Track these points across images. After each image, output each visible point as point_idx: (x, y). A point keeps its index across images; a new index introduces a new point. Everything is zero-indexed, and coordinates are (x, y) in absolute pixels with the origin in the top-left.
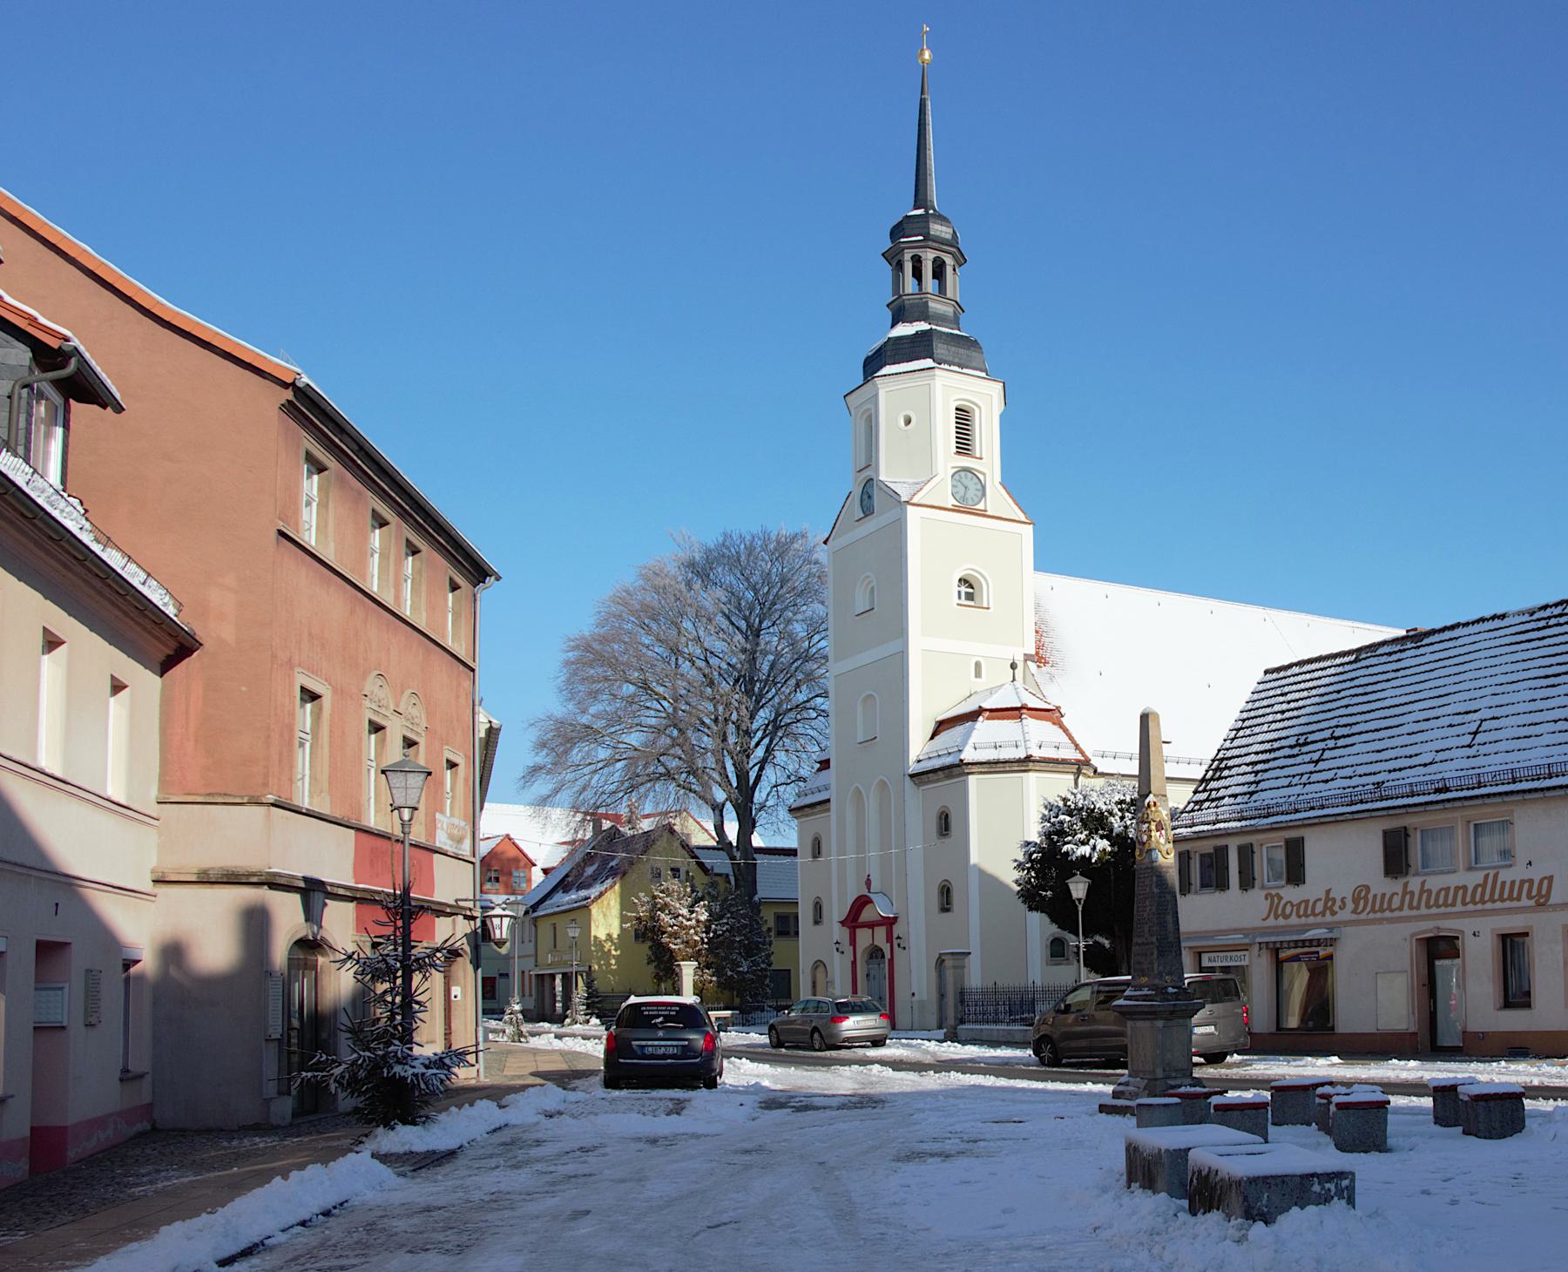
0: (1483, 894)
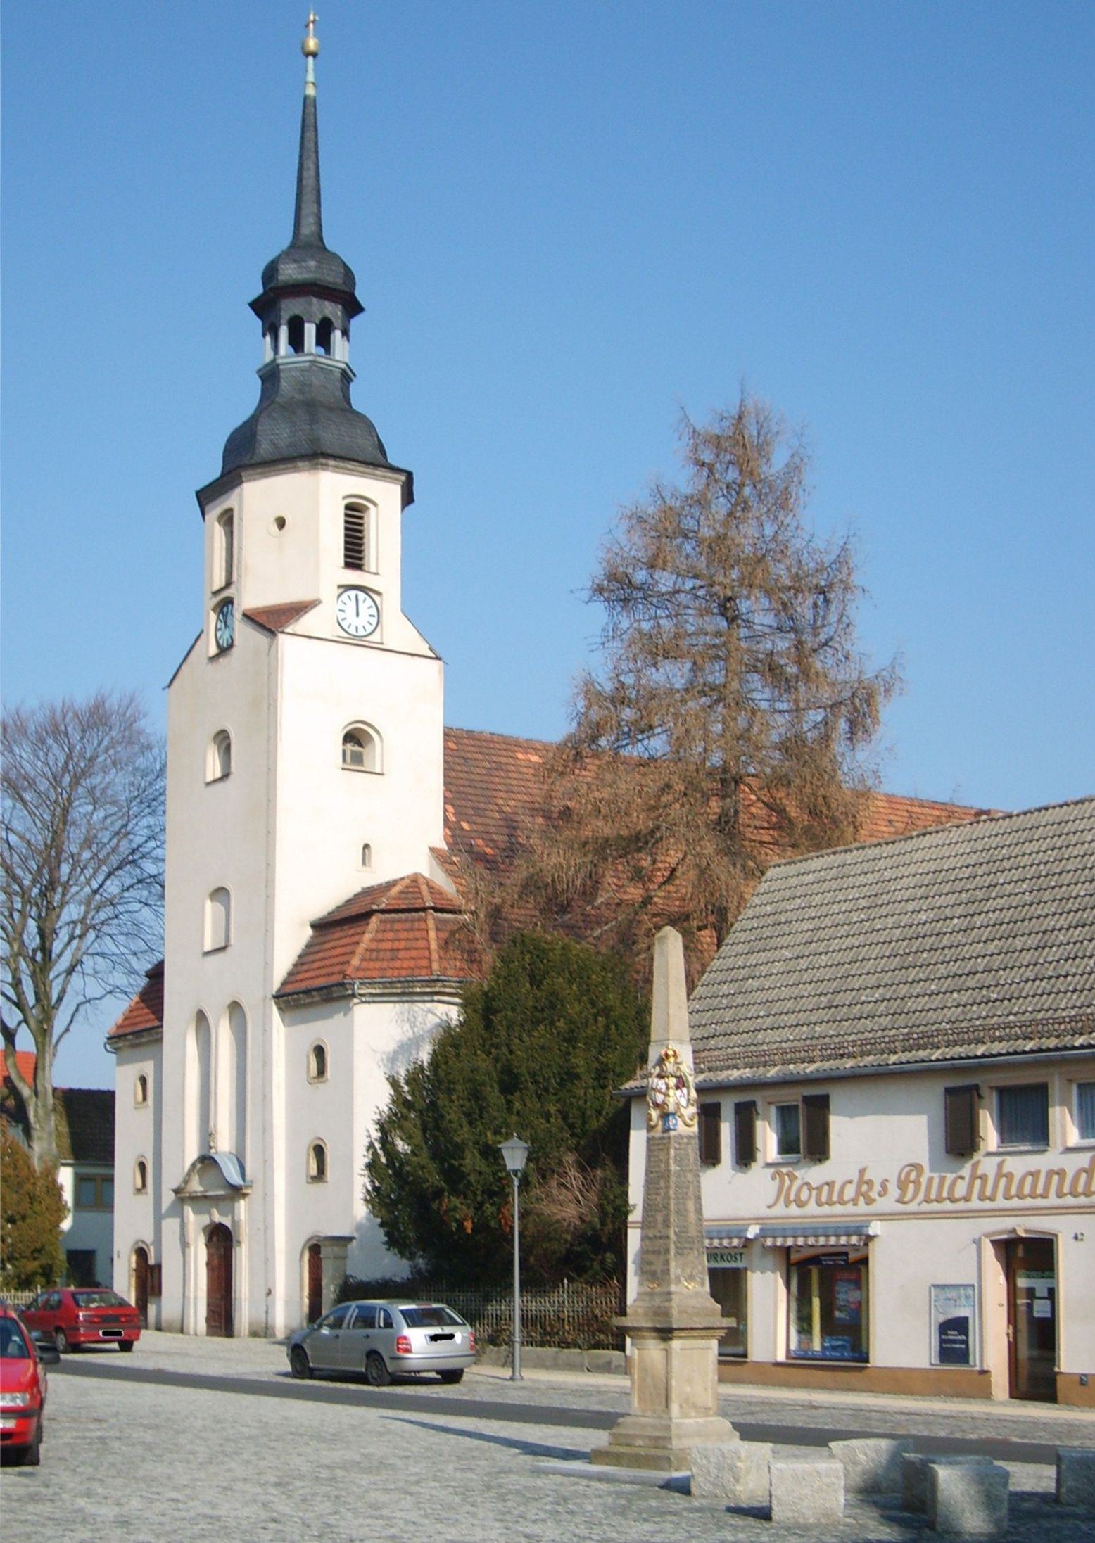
0: (1034, 1186)
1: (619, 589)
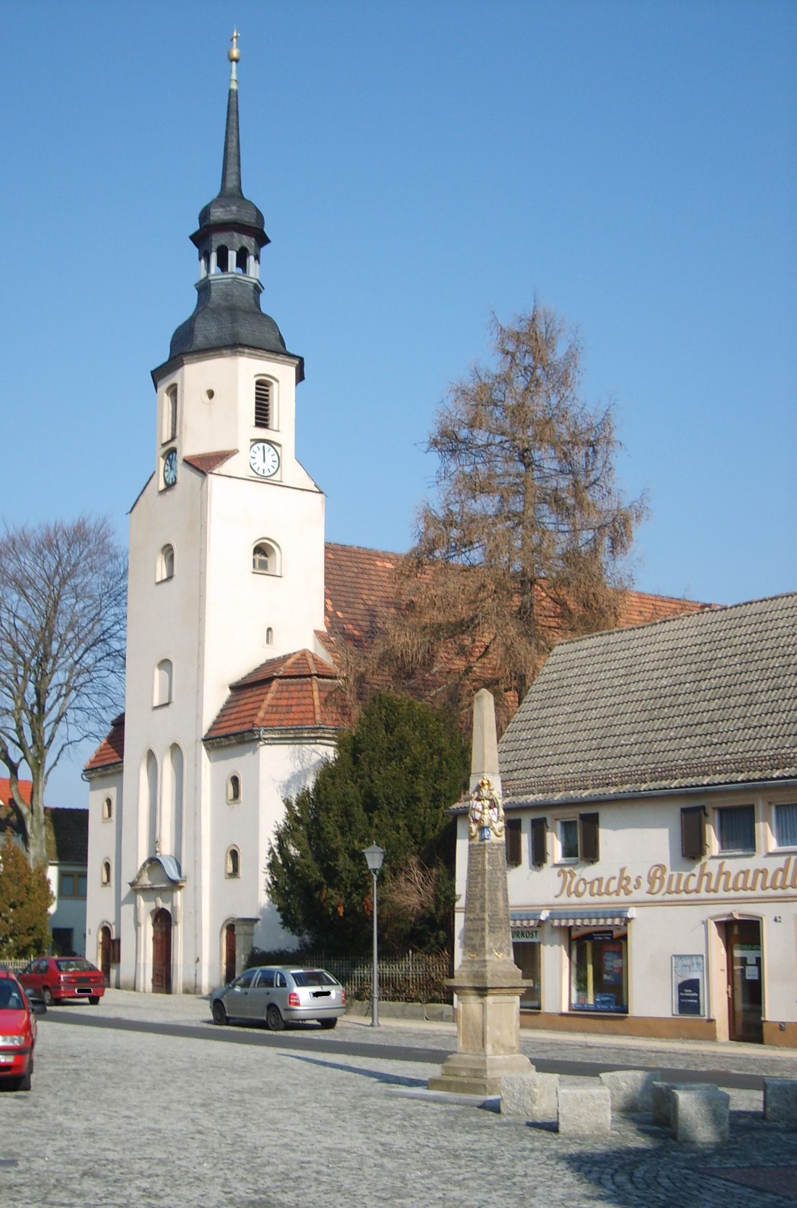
0: (745, 881)
1: (449, 442)
